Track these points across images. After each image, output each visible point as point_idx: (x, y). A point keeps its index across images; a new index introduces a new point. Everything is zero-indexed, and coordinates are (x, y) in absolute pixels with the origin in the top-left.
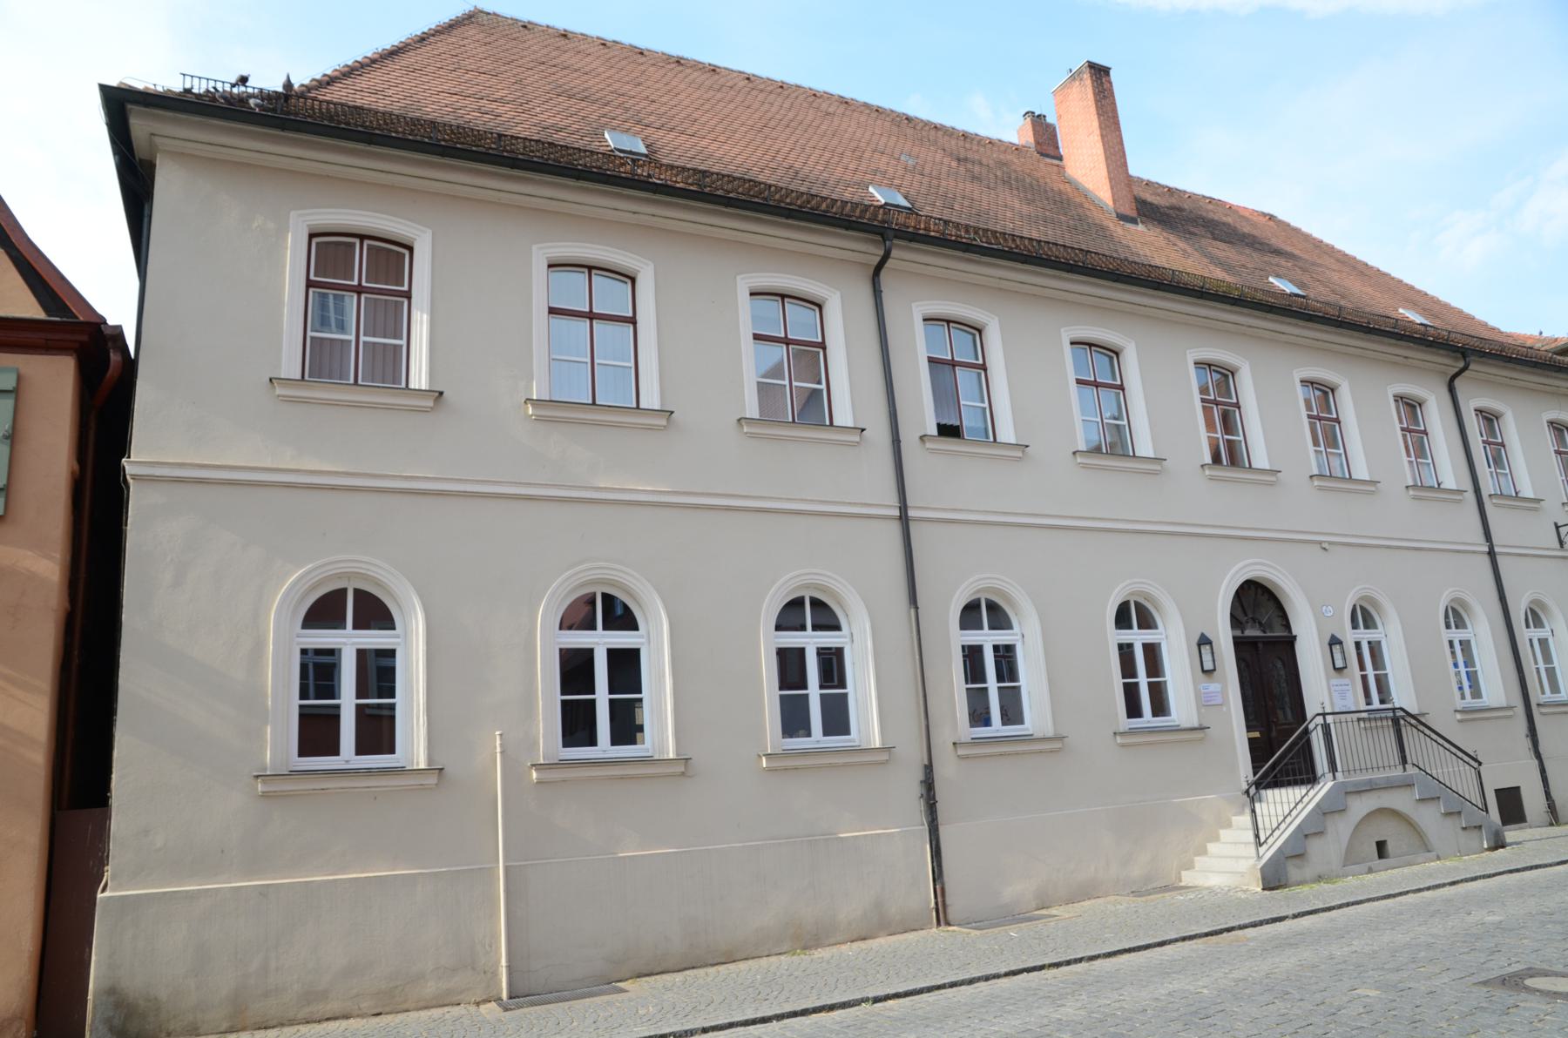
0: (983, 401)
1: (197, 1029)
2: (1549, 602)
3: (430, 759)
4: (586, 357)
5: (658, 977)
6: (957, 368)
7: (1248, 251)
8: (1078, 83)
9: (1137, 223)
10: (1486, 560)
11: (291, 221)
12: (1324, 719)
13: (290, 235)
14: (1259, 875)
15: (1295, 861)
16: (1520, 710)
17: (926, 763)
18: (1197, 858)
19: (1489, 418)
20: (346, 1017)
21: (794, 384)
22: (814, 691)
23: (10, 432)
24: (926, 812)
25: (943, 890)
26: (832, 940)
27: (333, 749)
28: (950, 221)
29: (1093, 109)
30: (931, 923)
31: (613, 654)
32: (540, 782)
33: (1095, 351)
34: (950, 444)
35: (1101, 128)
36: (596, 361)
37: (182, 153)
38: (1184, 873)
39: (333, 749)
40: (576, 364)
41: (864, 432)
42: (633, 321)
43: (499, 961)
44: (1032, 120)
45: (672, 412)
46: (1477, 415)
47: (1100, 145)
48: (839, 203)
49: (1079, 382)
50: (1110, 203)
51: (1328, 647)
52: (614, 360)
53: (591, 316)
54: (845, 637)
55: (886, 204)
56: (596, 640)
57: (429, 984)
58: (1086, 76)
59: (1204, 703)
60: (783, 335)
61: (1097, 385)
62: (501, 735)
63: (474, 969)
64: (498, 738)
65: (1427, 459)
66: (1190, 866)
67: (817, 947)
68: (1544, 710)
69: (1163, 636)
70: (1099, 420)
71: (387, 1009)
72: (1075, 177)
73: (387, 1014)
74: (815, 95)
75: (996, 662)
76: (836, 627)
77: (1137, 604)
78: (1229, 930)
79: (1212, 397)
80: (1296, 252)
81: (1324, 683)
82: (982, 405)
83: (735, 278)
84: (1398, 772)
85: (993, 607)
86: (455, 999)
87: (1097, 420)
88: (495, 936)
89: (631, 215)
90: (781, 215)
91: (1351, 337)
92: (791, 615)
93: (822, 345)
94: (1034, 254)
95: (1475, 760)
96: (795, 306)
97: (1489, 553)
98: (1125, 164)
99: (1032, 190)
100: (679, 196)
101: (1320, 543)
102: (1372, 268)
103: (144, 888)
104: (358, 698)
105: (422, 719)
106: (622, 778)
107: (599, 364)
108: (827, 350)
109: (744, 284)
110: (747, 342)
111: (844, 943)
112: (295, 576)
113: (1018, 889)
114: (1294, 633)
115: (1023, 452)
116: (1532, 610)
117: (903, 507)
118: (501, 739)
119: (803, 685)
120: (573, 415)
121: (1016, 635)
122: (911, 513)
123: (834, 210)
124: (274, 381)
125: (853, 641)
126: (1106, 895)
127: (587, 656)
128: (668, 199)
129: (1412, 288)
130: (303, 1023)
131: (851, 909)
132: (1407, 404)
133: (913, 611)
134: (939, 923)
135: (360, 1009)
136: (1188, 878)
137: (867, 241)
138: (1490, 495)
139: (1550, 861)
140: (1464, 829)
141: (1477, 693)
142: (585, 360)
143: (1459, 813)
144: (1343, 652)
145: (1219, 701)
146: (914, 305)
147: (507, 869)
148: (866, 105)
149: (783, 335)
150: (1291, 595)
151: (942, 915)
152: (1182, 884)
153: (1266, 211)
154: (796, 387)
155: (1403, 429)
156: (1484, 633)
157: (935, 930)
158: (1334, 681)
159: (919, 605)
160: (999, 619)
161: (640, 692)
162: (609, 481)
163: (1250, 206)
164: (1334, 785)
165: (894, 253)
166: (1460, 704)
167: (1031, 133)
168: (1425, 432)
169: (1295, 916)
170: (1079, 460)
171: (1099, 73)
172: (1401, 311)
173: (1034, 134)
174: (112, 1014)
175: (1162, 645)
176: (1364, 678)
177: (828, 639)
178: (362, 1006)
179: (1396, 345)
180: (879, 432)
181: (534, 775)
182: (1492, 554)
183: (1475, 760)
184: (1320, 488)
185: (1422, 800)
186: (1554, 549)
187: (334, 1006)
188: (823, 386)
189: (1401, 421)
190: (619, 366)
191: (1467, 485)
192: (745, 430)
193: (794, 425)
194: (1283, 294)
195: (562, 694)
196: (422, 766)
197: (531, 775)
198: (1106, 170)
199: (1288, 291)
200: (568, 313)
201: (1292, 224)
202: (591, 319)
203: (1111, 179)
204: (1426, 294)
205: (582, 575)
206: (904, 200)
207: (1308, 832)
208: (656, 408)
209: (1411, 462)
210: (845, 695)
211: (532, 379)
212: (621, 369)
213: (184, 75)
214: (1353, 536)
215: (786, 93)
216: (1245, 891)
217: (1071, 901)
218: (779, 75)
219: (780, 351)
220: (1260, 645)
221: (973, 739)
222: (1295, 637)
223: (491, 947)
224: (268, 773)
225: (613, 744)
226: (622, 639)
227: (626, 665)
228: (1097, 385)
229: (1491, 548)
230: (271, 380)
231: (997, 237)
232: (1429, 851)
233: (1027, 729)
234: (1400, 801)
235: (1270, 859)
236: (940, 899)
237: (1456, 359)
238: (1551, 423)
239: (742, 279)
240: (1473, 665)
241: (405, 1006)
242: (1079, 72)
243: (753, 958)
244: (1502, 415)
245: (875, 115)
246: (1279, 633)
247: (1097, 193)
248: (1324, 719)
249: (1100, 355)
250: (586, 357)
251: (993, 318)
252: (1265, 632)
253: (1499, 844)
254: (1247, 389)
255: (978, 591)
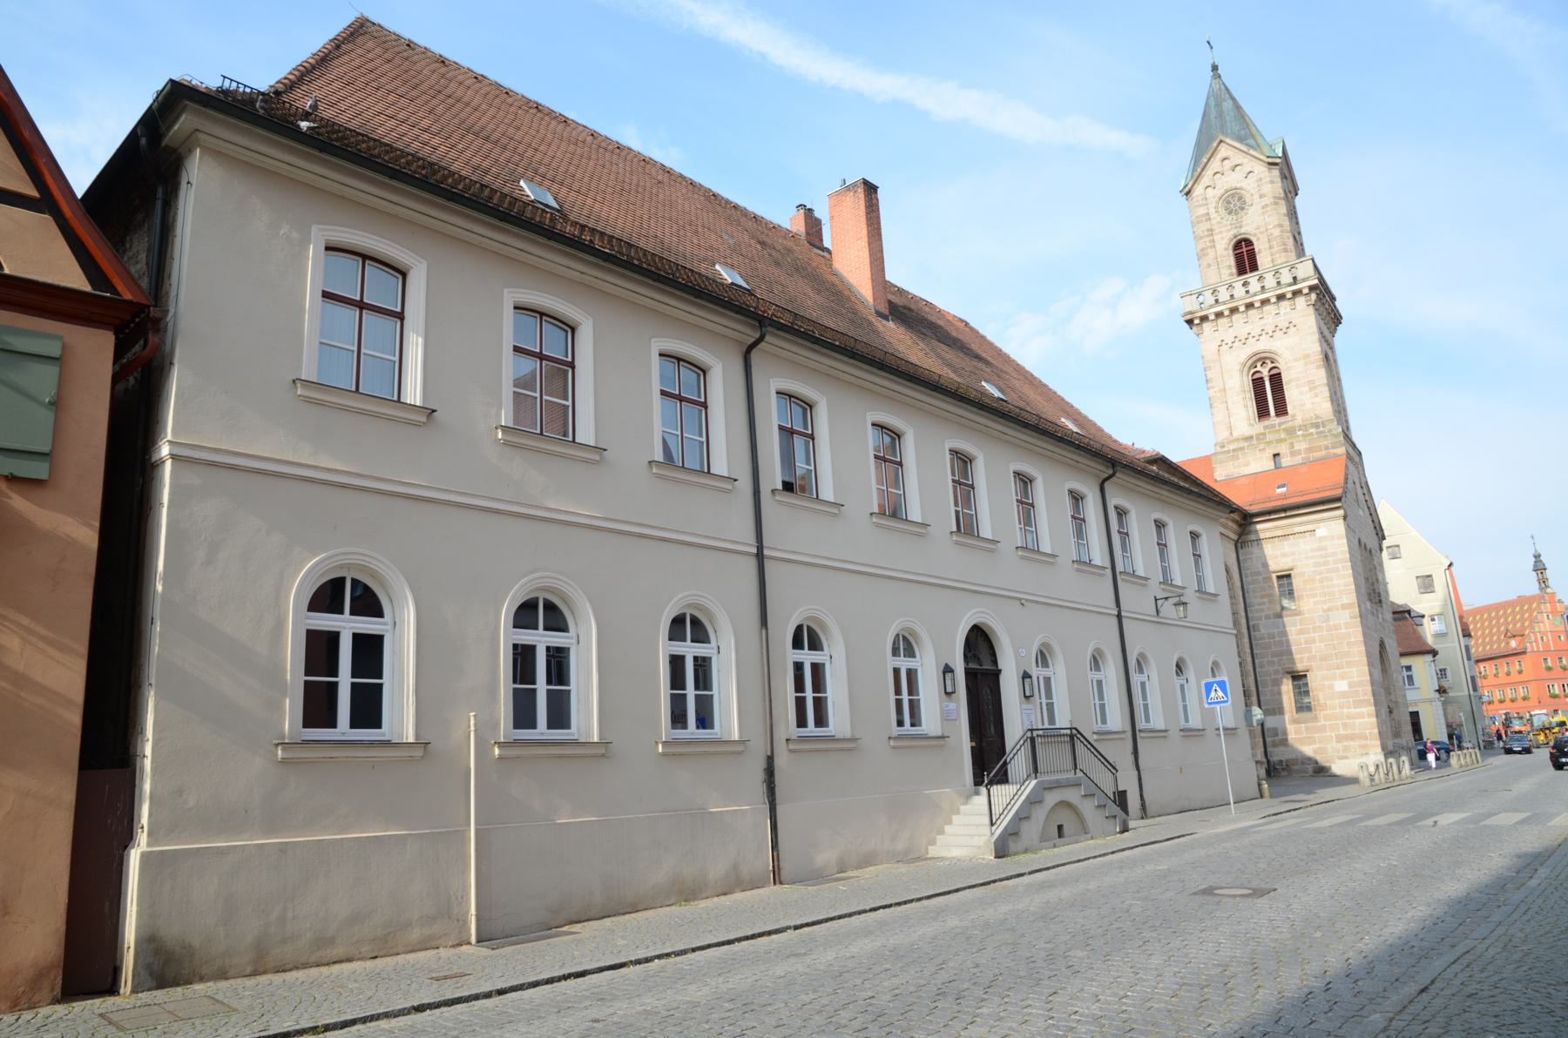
0: (701, 436)
1: (226, 973)
2: (1219, 660)
3: (417, 735)
4: (353, 345)
5: (586, 924)
6: (795, 435)
7: (961, 355)
8: (852, 194)
9: (888, 320)
10: (1115, 620)
11: (313, 234)
12: (1032, 734)
13: (311, 246)
14: (993, 846)
15: (1013, 837)
16: (1129, 734)
17: (769, 754)
18: (938, 837)
19: (1121, 513)
20: (349, 960)
21: (545, 397)
22: (541, 686)
23: (55, 398)
24: (767, 794)
25: (778, 855)
26: (704, 895)
27: (332, 723)
28: (587, 226)
29: (863, 219)
30: (770, 882)
31: (358, 639)
32: (501, 758)
33: (546, 321)
34: (787, 498)
35: (869, 237)
36: (363, 350)
37: (220, 152)
38: (930, 847)
39: (332, 723)
40: (337, 349)
41: (435, 413)
42: (400, 316)
43: (468, 911)
44: (805, 213)
45: (434, 411)
46: (1015, 476)
47: (866, 251)
48: (478, 185)
49: (663, 393)
50: (871, 300)
51: (1021, 680)
52: (383, 353)
53: (361, 305)
54: (713, 649)
55: (732, 284)
56: (343, 624)
57: (415, 931)
58: (861, 190)
59: (947, 718)
60: (358, 298)
61: (681, 399)
62: (475, 716)
63: (449, 917)
64: (472, 718)
65: (1032, 527)
66: (933, 843)
67: (695, 899)
68: (1143, 735)
69: (919, 664)
70: (679, 433)
71: (382, 953)
72: (841, 271)
73: (381, 957)
74: (443, 62)
75: (547, 660)
76: (378, 613)
77: (808, 627)
78: (994, 881)
79: (882, 455)
80: (989, 359)
81: (1018, 706)
82: (700, 439)
83: (650, 340)
84: (1071, 775)
85: (550, 608)
86: (434, 944)
87: (676, 433)
88: (466, 889)
89: (578, 274)
90: (731, 310)
91: (1047, 442)
92: (328, 597)
93: (400, 316)
94: (671, 276)
95: (1114, 768)
96: (552, 326)
97: (757, 555)
98: (883, 270)
99: (799, 269)
100: (643, 275)
101: (1020, 599)
102: (1036, 378)
103: (177, 845)
104: (306, 675)
105: (412, 699)
106: (560, 756)
107: (365, 354)
108: (405, 322)
109: (511, 297)
110: (657, 396)
111: (713, 897)
112: (312, 562)
113: (826, 857)
114: (1000, 668)
115: (601, 455)
116: (1041, 652)
117: (760, 548)
118: (475, 720)
119: (333, 670)
120: (680, 477)
121: (826, 655)
122: (766, 552)
123: (460, 187)
124: (297, 382)
125: (579, 642)
126: (882, 864)
127: (333, 638)
128: (614, 267)
129: (1063, 400)
130: (314, 967)
131: (717, 870)
132: (1023, 481)
133: (764, 631)
134: (775, 883)
135: (360, 953)
136: (933, 851)
137: (746, 324)
138: (1120, 572)
139: (1161, 839)
140: (1107, 817)
141: (1104, 721)
142: (352, 348)
143: (1105, 806)
144: (953, 680)
145: (954, 717)
146: (771, 380)
147: (477, 831)
148: (681, 176)
149: (358, 298)
150: (1001, 638)
151: (777, 878)
152: (929, 856)
153: (963, 318)
154: (546, 401)
155: (954, 481)
156: (1111, 673)
157: (772, 887)
158: (1024, 706)
159: (769, 627)
160: (556, 620)
161: (381, 678)
162: (559, 504)
163: (952, 312)
164: (1037, 783)
165: (768, 338)
166: (896, 731)
167: (802, 224)
168: (1032, 505)
169: (1030, 873)
170: (874, 520)
171: (870, 189)
172: (1063, 420)
173: (806, 226)
174: (151, 960)
175: (571, 650)
176: (899, 703)
177: (556, 639)
178: (362, 950)
179: (1074, 453)
180: (745, 484)
181: (497, 751)
182: (1119, 616)
183: (1114, 768)
184: (1022, 557)
185: (1085, 796)
186: (1150, 616)
187: (339, 951)
188: (569, 403)
189: (953, 474)
190: (370, 355)
191: (1108, 564)
192: (654, 471)
193: (682, 469)
194: (992, 397)
195: (353, 677)
196: (411, 740)
197: (494, 751)
198: (869, 272)
199: (996, 395)
200: (372, 308)
201: (980, 332)
202: (361, 309)
203: (873, 281)
204: (1072, 406)
205: (342, 557)
206: (554, 201)
207: (1021, 817)
208: (591, 444)
209: (1021, 528)
210: (380, 686)
211: (501, 408)
212: (372, 358)
213: (225, 77)
214: (706, 537)
215: (510, 100)
216: (983, 859)
217: (859, 867)
218: (408, 33)
219: (531, 365)
220: (979, 676)
221: (799, 737)
222: (1000, 671)
223: (462, 898)
224: (286, 741)
225: (549, 728)
226: (367, 625)
227: (369, 651)
228: (681, 399)
229: (1119, 612)
230: (294, 381)
231: (621, 246)
232: (1086, 833)
233: (830, 731)
234: (1072, 796)
235: (1000, 835)
236: (776, 863)
237: (1107, 467)
238: (1071, 492)
239: (509, 292)
240: (1051, 698)
241: (395, 950)
242: (854, 185)
243: (651, 909)
244: (1129, 512)
245: (690, 187)
246: (987, 666)
247: (859, 289)
248: (1032, 734)
249: (549, 325)
250: (353, 345)
251: (588, 319)
252: (981, 665)
253: (1125, 830)
254: (910, 451)
255: (538, 589)
